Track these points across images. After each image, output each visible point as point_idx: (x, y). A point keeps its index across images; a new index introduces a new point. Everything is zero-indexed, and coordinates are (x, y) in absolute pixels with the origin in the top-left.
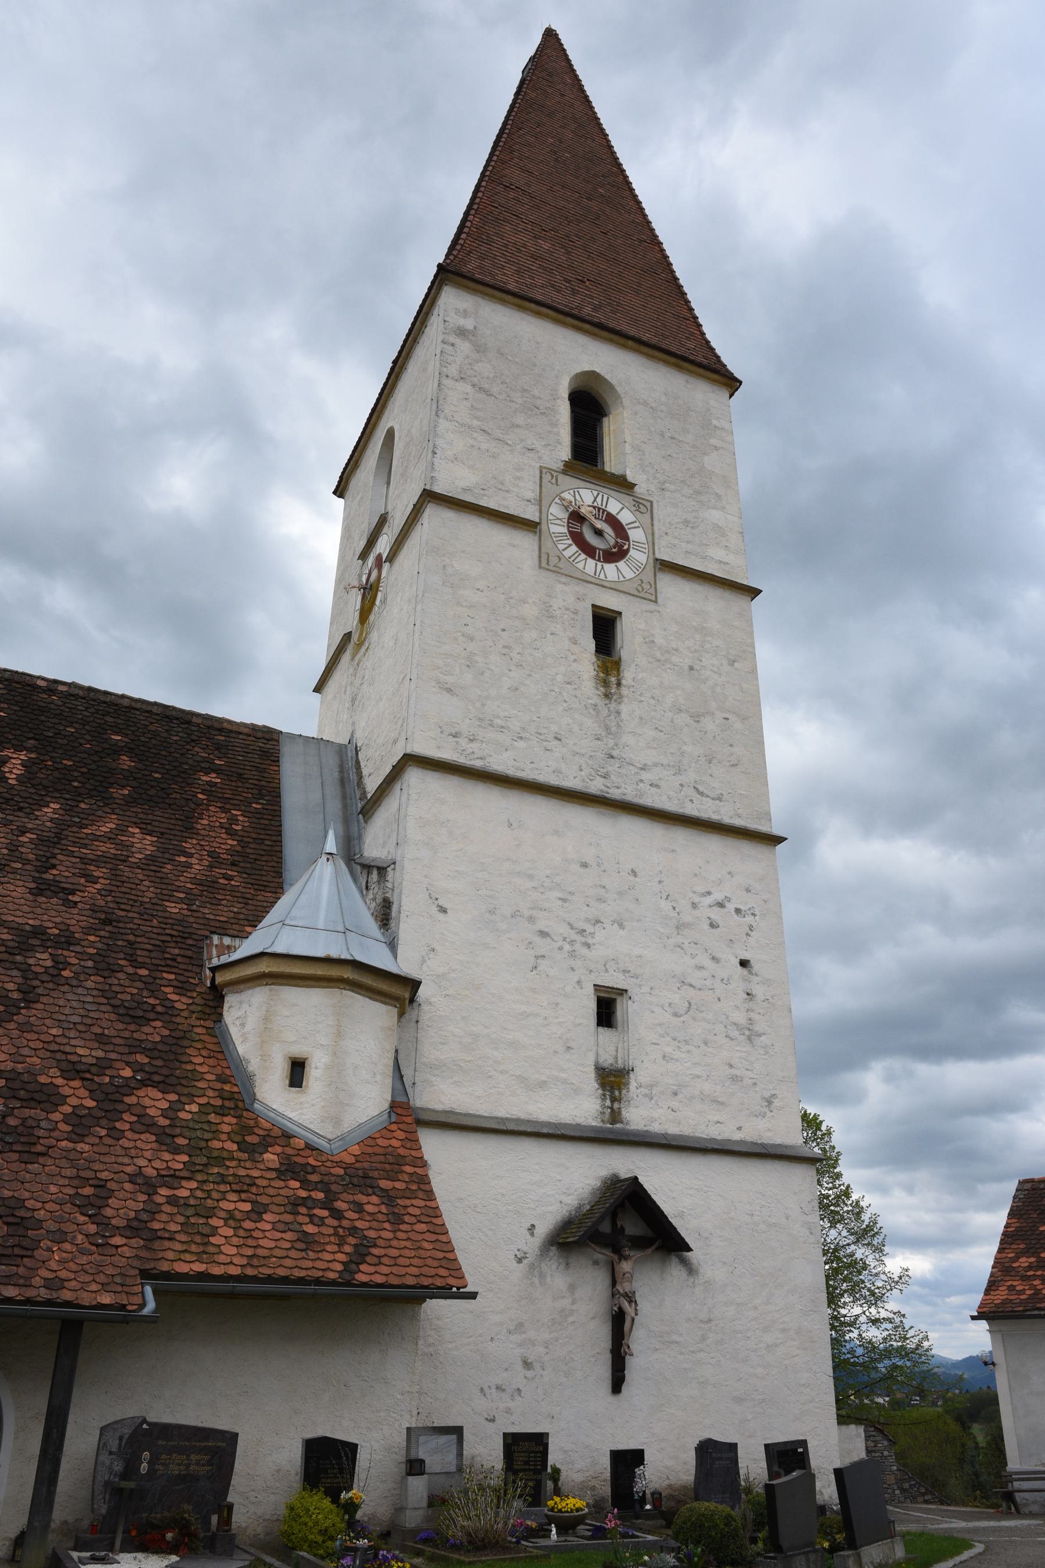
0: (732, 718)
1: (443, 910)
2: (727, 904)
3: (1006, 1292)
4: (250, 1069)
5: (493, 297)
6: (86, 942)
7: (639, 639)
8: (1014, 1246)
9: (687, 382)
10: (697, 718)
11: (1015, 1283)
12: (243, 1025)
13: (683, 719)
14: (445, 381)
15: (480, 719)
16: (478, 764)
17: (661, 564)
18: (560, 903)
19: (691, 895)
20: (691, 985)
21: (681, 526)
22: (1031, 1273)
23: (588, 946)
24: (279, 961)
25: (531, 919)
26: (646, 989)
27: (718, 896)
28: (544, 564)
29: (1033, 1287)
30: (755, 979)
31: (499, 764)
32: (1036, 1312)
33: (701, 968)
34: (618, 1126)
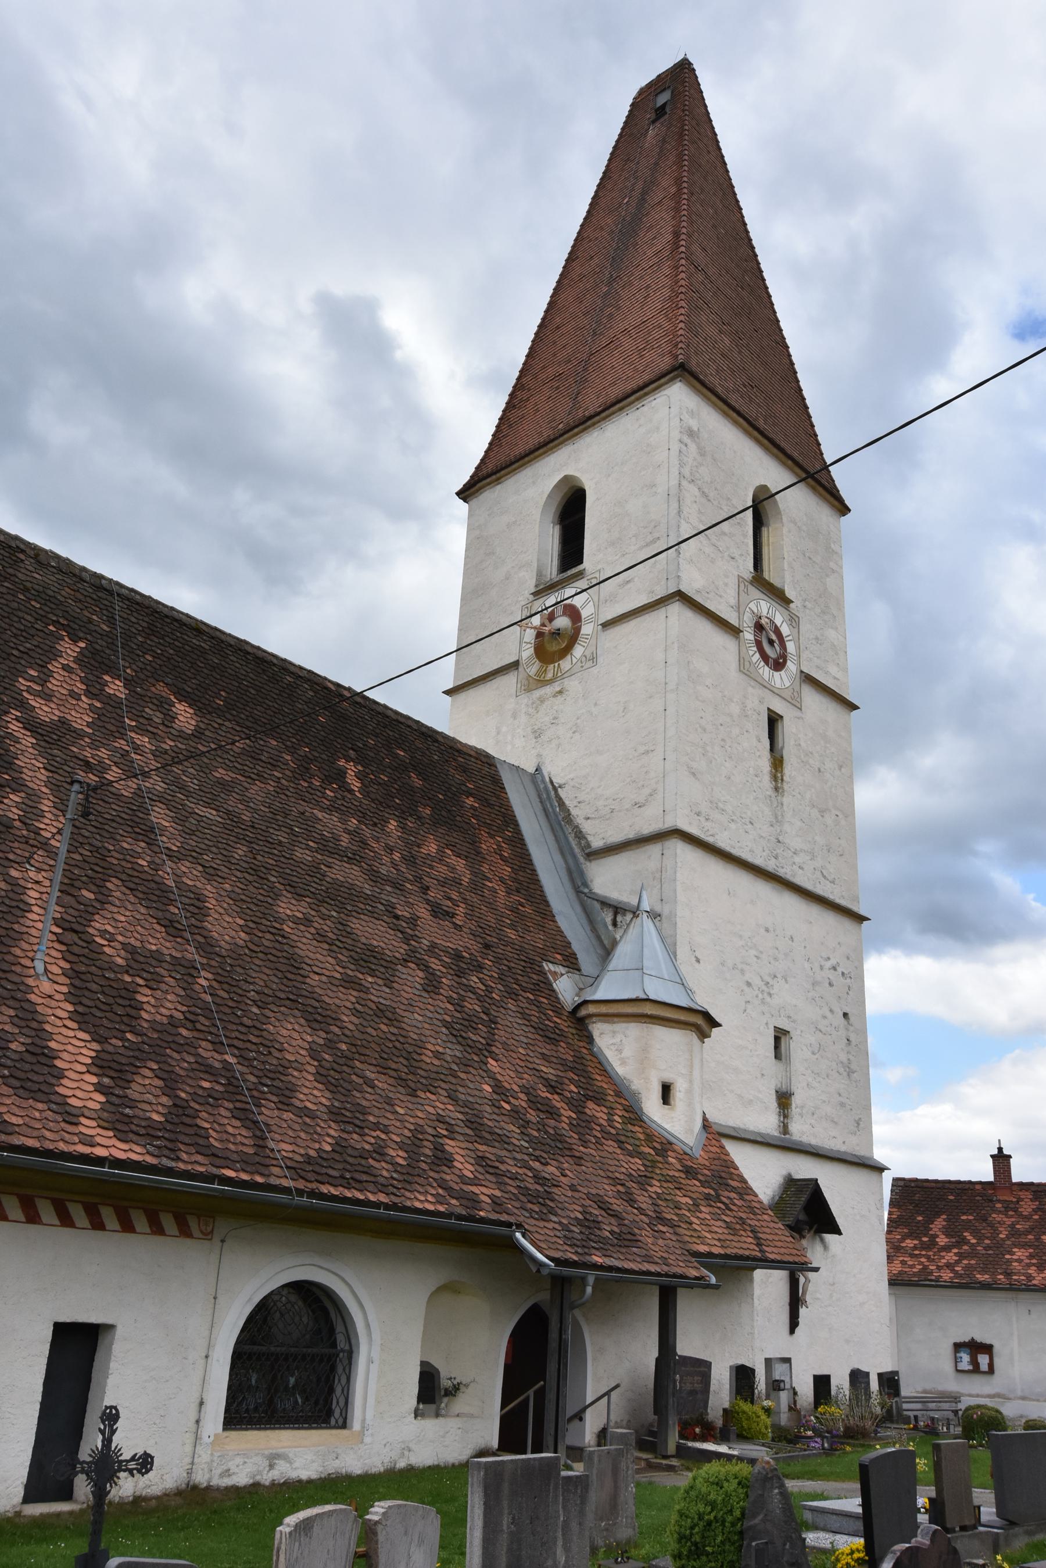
0: (841, 816)
1: (698, 961)
2: (838, 968)
3: (900, 1265)
4: (633, 1087)
5: (709, 399)
6: (33, 827)
7: (792, 742)
8: (898, 1230)
9: (818, 503)
10: (822, 812)
11: (906, 1259)
12: (620, 1051)
13: (815, 813)
14: (684, 483)
15: (711, 802)
16: (710, 840)
17: (805, 677)
18: (755, 959)
19: (820, 959)
20: (820, 1031)
21: (814, 642)
22: (917, 1252)
23: (770, 995)
24: (656, 1006)
25: (742, 972)
26: (799, 1032)
27: (833, 962)
28: (742, 669)
29: (921, 1263)
30: (851, 1028)
31: (723, 842)
32: (928, 1283)
33: (825, 1017)
34: (787, 1136)
